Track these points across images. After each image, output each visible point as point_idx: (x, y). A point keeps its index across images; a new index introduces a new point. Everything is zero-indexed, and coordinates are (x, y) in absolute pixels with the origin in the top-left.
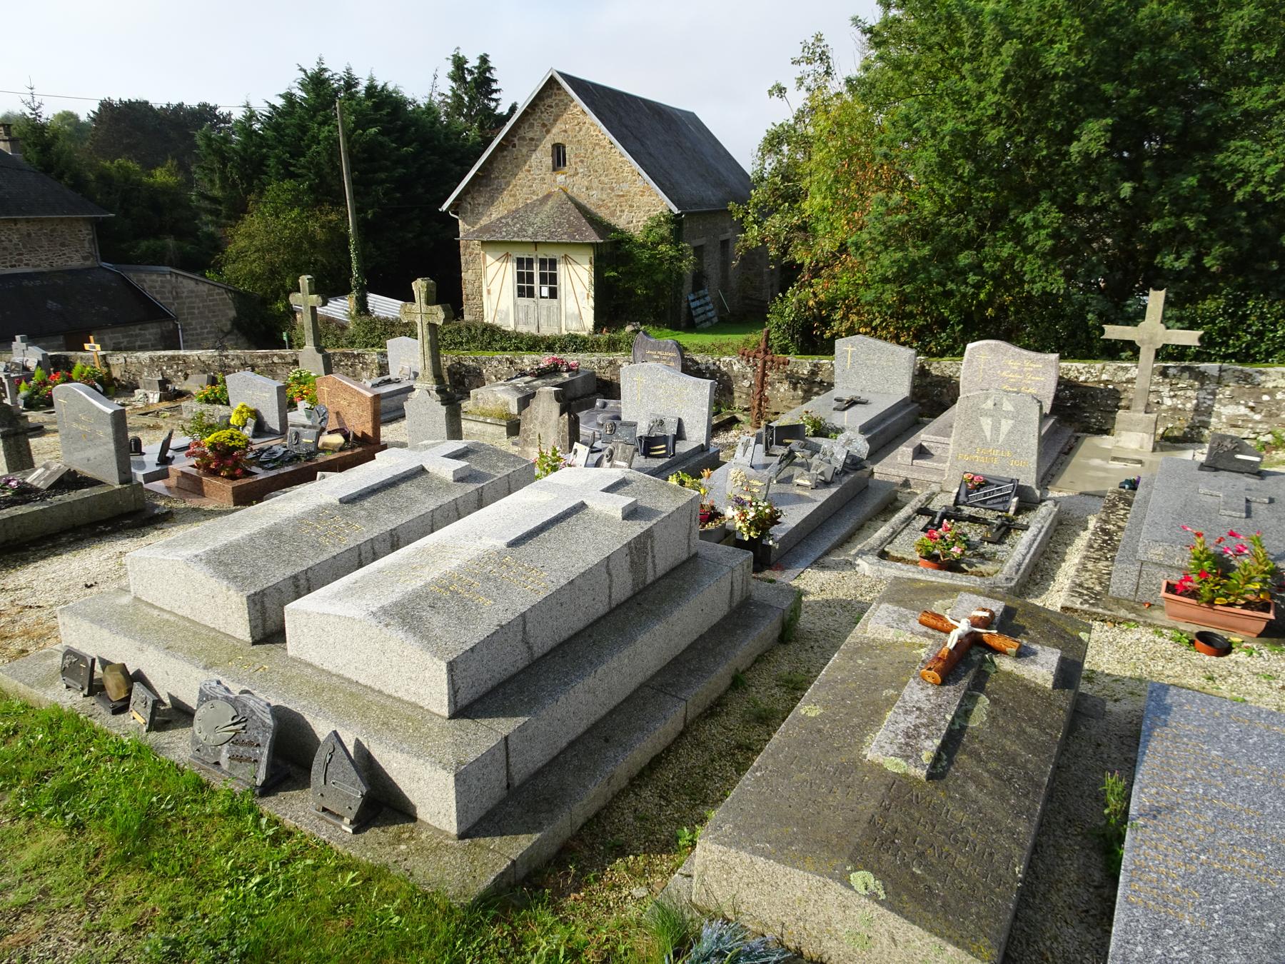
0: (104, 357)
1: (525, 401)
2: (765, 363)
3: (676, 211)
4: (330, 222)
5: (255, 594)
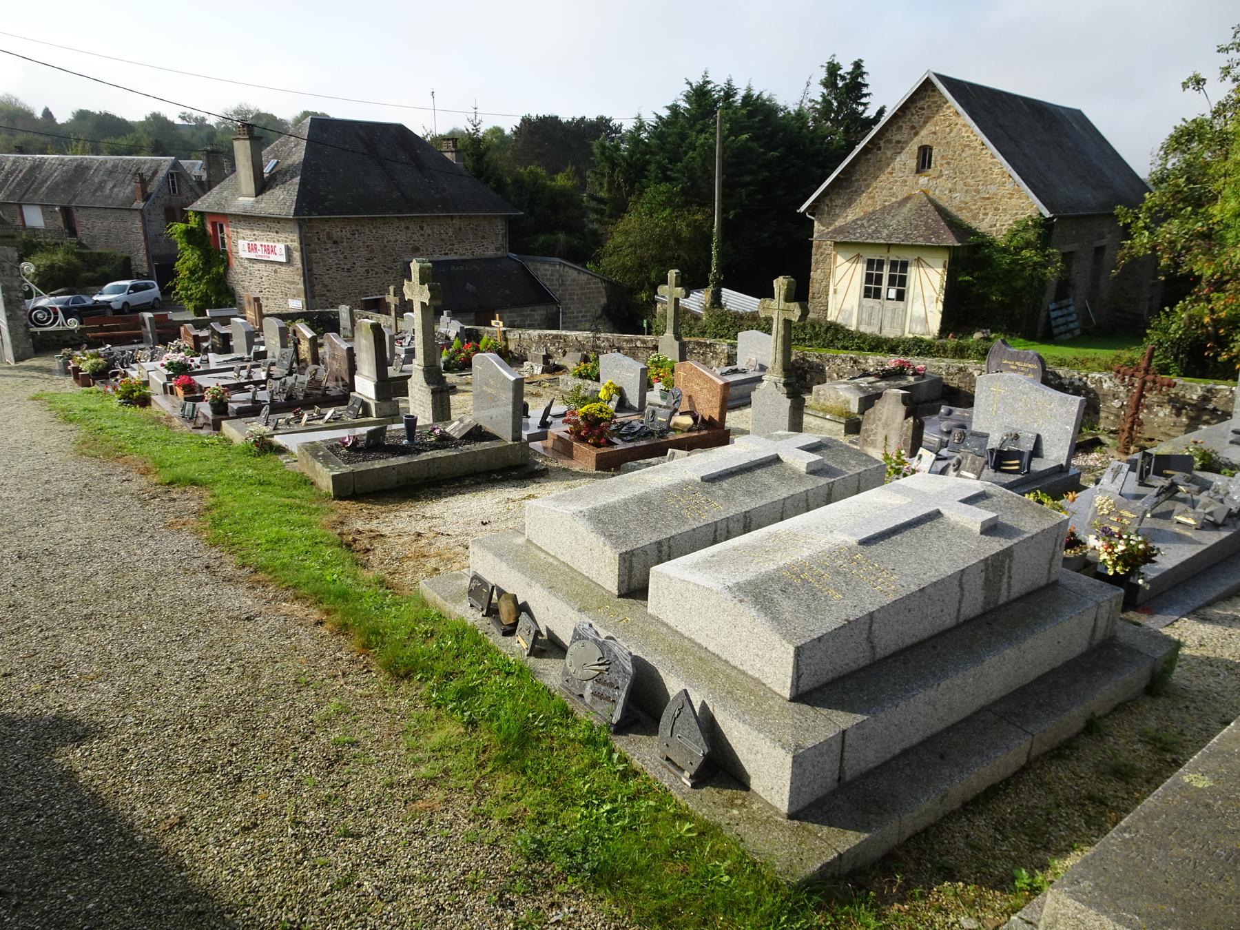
0: (504, 332)
1: (868, 401)
2: (1144, 383)
3: (1047, 214)
4: (696, 221)
5: (626, 553)
